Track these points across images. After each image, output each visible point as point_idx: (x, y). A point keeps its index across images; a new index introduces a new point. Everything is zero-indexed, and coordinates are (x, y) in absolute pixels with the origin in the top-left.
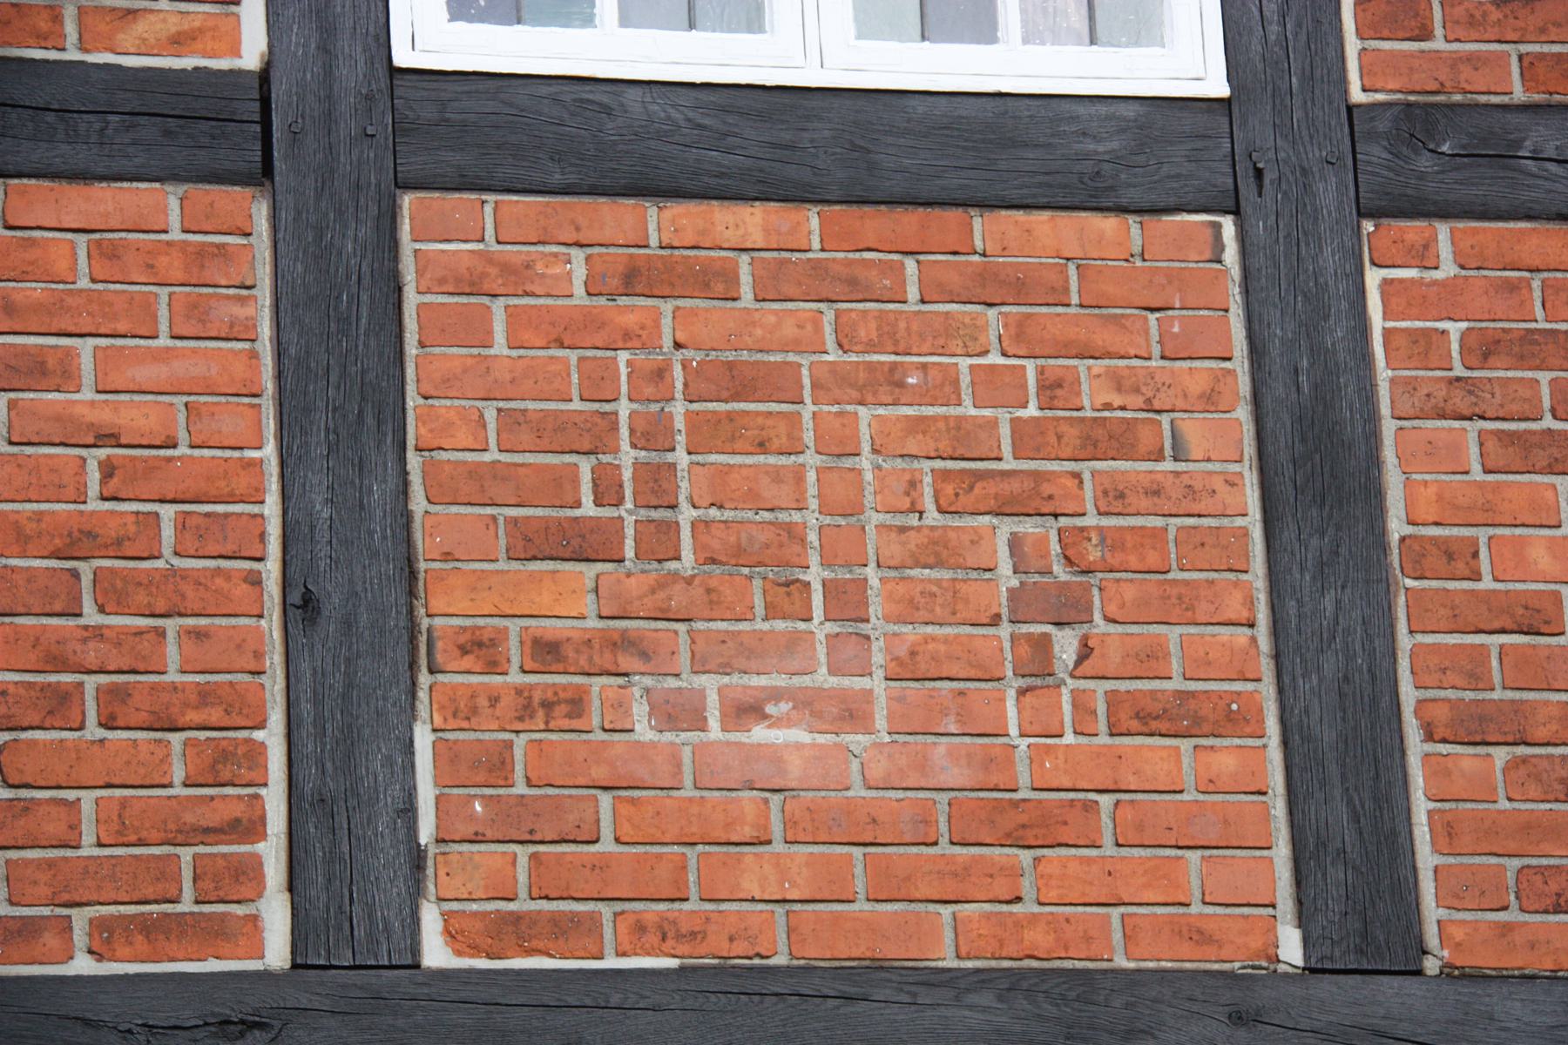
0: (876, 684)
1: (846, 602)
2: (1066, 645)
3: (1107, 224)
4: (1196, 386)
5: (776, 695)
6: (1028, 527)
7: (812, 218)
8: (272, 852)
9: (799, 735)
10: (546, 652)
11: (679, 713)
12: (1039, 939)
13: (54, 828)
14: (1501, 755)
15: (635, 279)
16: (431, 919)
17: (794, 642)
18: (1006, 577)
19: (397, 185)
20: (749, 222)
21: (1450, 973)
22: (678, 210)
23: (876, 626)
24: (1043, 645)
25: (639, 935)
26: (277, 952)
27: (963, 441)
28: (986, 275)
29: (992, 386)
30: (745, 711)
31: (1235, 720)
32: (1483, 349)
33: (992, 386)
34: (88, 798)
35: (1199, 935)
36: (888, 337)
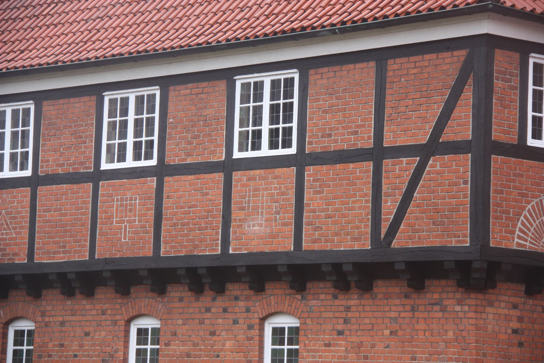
0: (264, 222)
1: (262, 215)
2: (278, 217)
3: (285, 169)
4: (291, 187)
5: (256, 224)
6: (276, 204)
7: (263, 170)
8: (220, 242)
9: (257, 228)
10: (240, 220)
11: (249, 226)
12: (273, 248)
13: (370, 119)
14: (310, 226)
15: (249, 179)
16: (231, 248)
17: (258, 218)
18: (274, 210)
19: (348, 70)
20: (257, 172)
21: (305, 250)
22: (253, 171)
23: (264, 216)
24: (276, 217)
25: (245, 249)
26: (219, 252)
27: (272, 195)
28: (276, 176)
29: (275, 189)
30: (254, 226)
31: (290, 224)
32: (314, 181)
33: (275, 189)
34: (208, 237)
35: (285, 247)
36: (267, 184)
